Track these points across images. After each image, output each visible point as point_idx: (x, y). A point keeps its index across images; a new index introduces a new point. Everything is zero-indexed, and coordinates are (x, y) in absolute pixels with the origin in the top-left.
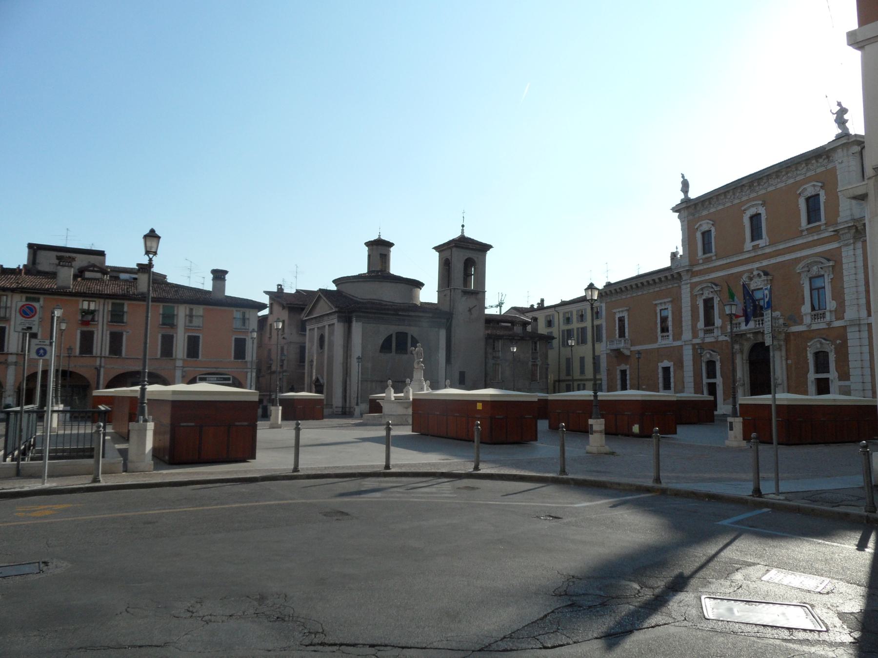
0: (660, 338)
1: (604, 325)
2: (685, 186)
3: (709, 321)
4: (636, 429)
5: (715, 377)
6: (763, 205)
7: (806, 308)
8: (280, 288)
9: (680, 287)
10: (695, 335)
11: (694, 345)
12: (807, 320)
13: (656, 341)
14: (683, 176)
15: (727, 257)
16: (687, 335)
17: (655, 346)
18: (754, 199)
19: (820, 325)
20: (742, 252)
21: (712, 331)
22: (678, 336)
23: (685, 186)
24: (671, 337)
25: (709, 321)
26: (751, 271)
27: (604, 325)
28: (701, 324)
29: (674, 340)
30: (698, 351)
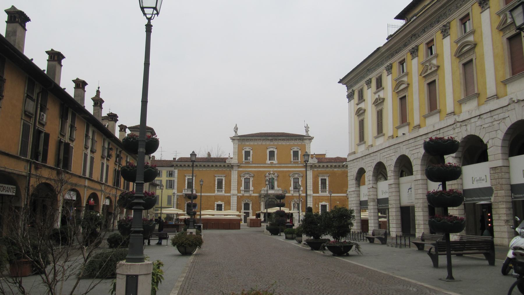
0: (216, 191)
1: (176, 181)
2: (236, 129)
3: (247, 187)
4: (289, 221)
5: (249, 209)
6: (276, 148)
7: (292, 188)
8: (193, 154)
9: (231, 171)
10: (239, 191)
11: (238, 196)
12: (292, 192)
13: (214, 192)
14: (98, 92)
15: (259, 164)
16: (234, 191)
17: (317, 195)
18: (274, 145)
19: (247, 194)
20: (266, 164)
21: (249, 191)
22: (228, 190)
23: (236, 129)
24: (223, 192)
25: (247, 187)
26: (270, 171)
27: (176, 181)
28: (242, 188)
29: (225, 193)
30: (239, 199)
